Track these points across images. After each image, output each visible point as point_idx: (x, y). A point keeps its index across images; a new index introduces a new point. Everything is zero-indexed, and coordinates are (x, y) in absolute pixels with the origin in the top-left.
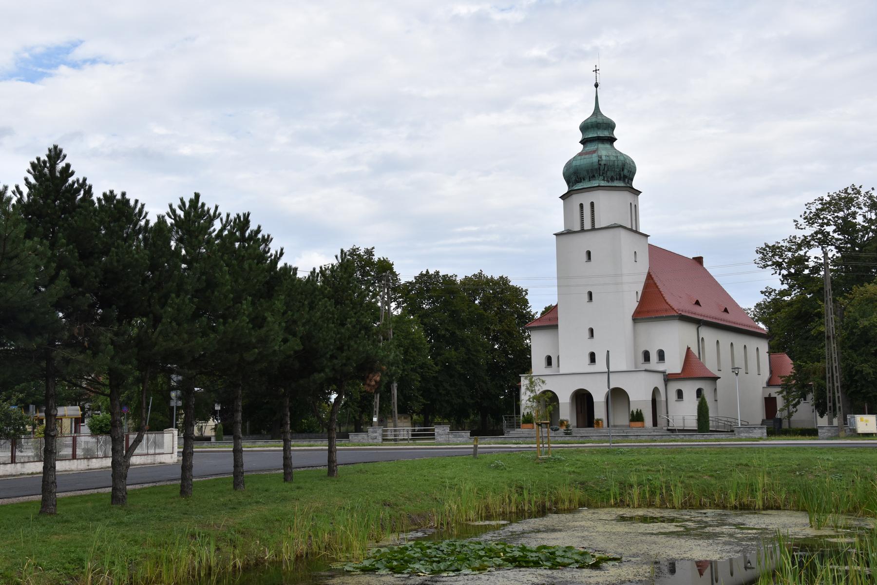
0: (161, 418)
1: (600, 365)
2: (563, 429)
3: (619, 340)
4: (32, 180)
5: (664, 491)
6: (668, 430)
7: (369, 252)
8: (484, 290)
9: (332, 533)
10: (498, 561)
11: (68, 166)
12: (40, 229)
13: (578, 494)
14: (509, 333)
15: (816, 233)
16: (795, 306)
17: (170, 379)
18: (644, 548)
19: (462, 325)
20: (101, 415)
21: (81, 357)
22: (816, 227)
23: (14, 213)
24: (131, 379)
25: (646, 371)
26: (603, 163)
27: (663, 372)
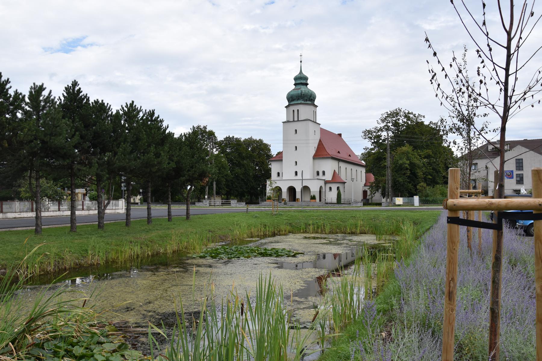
0: (118, 194)
1: (299, 176)
2: (283, 202)
4: (65, 95)
7: (205, 127)
9: (188, 242)
10: (255, 254)
11: (80, 89)
12: (68, 115)
13: (288, 228)
15: (385, 126)
17: (121, 178)
18: (313, 249)
19: (243, 159)
20: (94, 193)
21: (85, 168)
22: (385, 124)
23: (58, 108)
24: (105, 178)
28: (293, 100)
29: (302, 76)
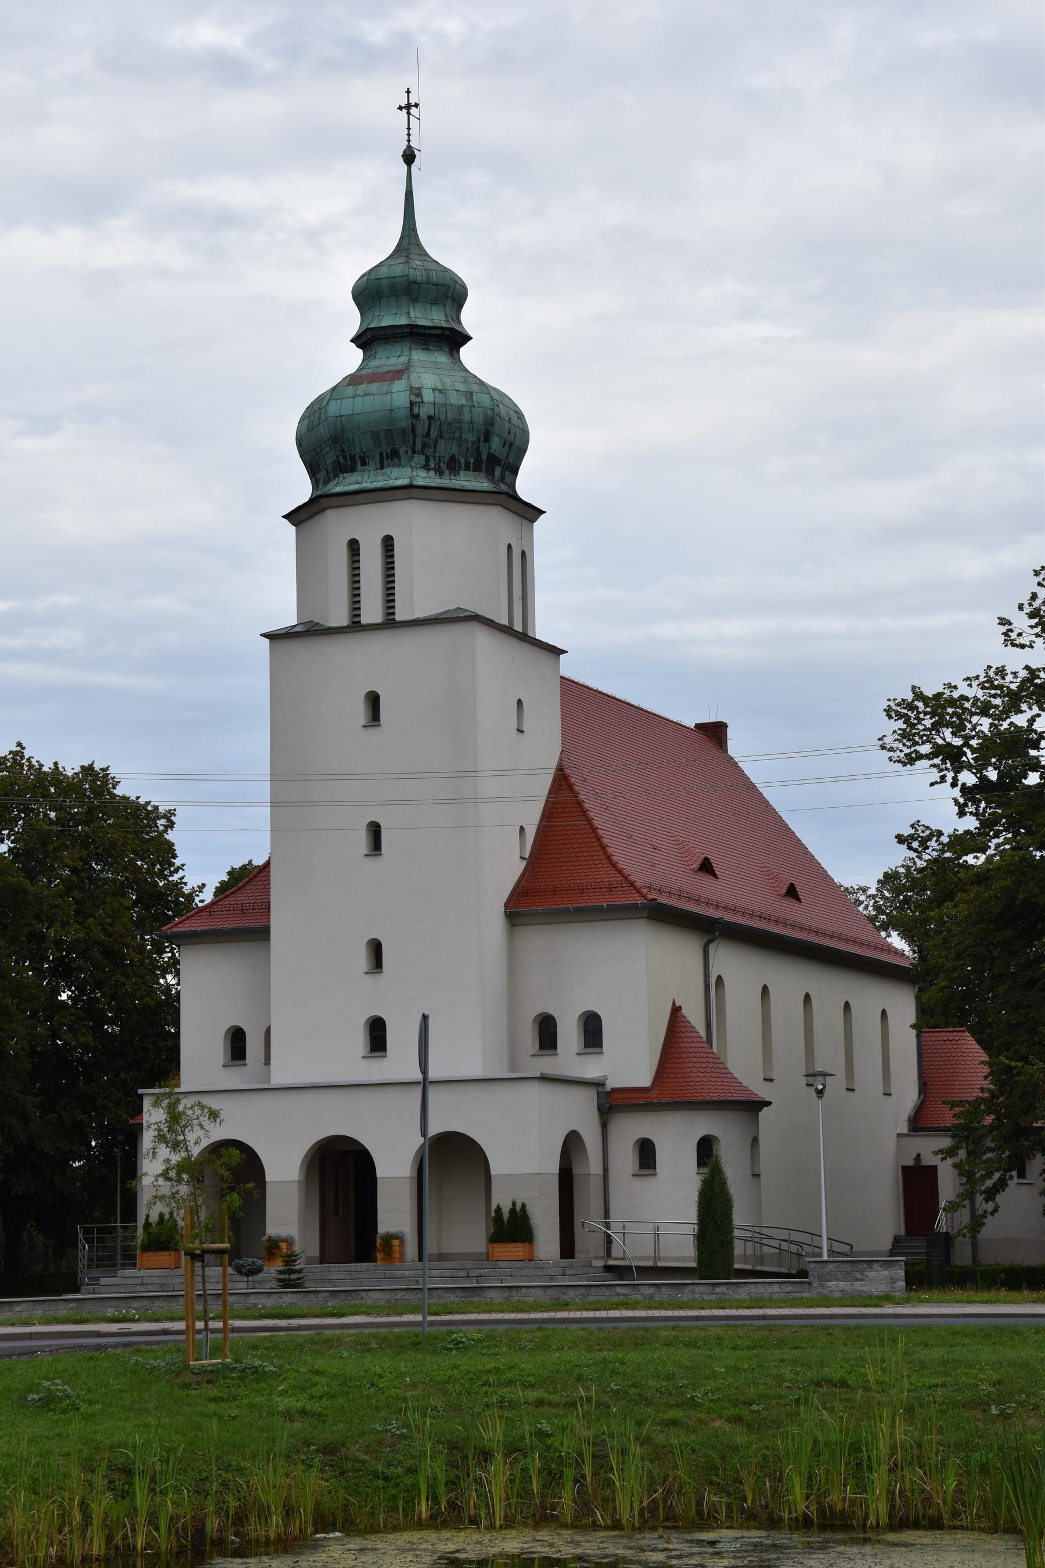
1: (400, 1060)
2: (274, 1268)
3: (461, 983)
5: (588, 1471)
6: (608, 1269)
8: (27, 810)
13: (314, 1485)
14: (108, 952)
16: (997, 885)
25: (544, 1078)
26: (424, 412)
27: (597, 1085)
28: (348, 464)
29: (416, 270)
